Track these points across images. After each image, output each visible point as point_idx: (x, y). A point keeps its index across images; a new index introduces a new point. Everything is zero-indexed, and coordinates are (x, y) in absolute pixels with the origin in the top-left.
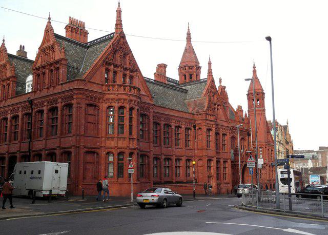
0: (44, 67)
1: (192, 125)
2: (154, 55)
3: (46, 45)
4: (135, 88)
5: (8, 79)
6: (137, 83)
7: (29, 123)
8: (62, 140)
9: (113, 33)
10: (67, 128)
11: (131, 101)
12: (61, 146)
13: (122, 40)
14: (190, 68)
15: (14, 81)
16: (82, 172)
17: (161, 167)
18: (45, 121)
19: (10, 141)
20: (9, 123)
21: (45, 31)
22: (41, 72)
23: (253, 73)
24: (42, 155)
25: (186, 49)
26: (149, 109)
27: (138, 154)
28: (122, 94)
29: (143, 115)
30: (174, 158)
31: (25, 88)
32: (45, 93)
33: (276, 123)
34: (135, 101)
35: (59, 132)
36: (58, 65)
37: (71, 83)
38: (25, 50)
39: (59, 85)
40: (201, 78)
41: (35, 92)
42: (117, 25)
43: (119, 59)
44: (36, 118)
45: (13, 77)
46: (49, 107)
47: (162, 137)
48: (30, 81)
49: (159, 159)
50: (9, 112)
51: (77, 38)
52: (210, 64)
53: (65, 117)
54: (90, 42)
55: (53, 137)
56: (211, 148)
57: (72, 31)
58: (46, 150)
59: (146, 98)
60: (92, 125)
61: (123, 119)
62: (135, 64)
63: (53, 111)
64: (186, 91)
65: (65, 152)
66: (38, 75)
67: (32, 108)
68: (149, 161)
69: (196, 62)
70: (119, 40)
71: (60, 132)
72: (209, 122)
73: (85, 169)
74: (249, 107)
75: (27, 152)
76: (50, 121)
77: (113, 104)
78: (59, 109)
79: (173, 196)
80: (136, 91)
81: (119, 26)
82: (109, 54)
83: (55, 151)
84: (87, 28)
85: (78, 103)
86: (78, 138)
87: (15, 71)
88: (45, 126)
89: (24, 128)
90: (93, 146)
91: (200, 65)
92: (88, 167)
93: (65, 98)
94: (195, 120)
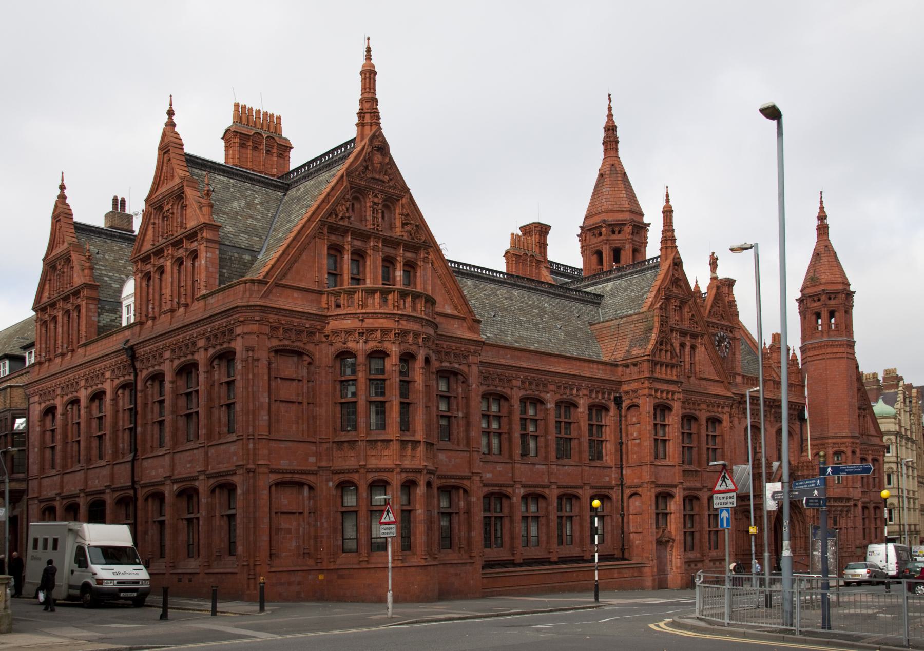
0: (159, 253)
1: (609, 398)
3: (163, 190)
4: (416, 296)
5: (76, 293)
6: (425, 281)
8: (212, 451)
10: (224, 419)
11: (405, 333)
12: (210, 471)
13: (378, 158)
14: (615, 229)
15: (94, 299)
16: (265, 538)
19: (89, 460)
21: (160, 149)
22: (154, 266)
23: (819, 235)
24: (78, 505)
25: (601, 175)
27: (429, 484)
29: (446, 374)
30: (553, 493)
31: (121, 317)
32: (164, 324)
34: (416, 335)
35: (203, 432)
36: (195, 244)
38: (127, 212)
39: (198, 299)
40: (648, 257)
43: (369, 215)
44: (146, 397)
45: (86, 286)
46: (176, 362)
47: (552, 437)
49: (508, 497)
50: (82, 383)
51: (266, 165)
52: (668, 212)
56: (667, 462)
57: (243, 145)
58: (175, 482)
60: (294, 407)
62: (421, 226)
63: (189, 374)
64: (596, 300)
65: (221, 486)
66: (148, 276)
67: (135, 370)
68: (469, 504)
69: (631, 211)
70: (369, 159)
71: (204, 432)
72: (664, 387)
73: (274, 531)
74: (803, 339)
76: (182, 402)
78: (201, 369)
79: (393, 590)
80: (420, 305)
81: (368, 118)
82: (337, 203)
83: (197, 483)
85: (249, 349)
86: (251, 446)
87: (92, 268)
89: (121, 423)
90: (295, 466)
91: (852, 289)
92: (283, 525)
93: (216, 336)
94: (620, 383)
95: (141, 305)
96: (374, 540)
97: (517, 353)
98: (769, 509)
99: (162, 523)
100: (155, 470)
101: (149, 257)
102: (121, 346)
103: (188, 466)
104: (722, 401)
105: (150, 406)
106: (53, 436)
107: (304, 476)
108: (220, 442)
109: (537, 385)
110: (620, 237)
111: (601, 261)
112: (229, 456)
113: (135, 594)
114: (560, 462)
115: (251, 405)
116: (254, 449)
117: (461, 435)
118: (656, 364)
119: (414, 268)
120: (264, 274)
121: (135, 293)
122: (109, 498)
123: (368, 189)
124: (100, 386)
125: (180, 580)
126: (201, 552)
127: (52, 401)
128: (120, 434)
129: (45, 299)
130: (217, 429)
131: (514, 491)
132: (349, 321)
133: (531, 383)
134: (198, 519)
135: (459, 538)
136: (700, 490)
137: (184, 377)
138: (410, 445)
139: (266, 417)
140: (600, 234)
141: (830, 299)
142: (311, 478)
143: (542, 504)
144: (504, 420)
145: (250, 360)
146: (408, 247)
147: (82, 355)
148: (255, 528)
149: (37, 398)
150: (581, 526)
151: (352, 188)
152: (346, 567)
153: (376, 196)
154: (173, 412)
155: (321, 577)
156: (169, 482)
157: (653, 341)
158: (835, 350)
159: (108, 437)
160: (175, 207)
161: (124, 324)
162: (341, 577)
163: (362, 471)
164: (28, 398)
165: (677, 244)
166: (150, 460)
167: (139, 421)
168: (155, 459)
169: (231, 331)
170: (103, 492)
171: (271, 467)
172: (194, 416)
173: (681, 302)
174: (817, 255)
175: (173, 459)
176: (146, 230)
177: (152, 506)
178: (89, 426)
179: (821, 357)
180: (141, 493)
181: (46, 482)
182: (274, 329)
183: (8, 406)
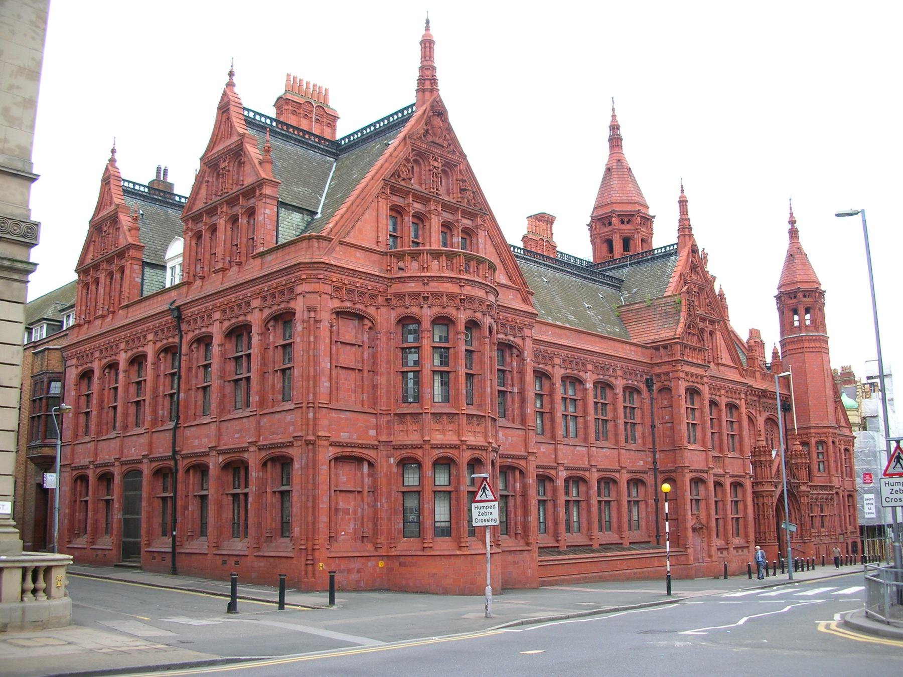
0: (212, 211)
2: (532, 182)
3: (220, 147)
6: (485, 249)
7: (173, 375)
8: (264, 421)
9: (411, 106)
10: (279, 386)
13: (437, 121)
14: (620, 226)
16: (324, 518)
17: (555, 506)
19: (125, 428)
20: (121, 376)
21: (219, 108)
24: (113, 475)
25: (608, 170)
26: (521, 329)
28: (440, 279)
29: (505, 347)
30: (594, 476)
35: (254, 398)
38: (170, 179)
39: (254, 257)
42: (421, 81)
46: (226, 324)
47: (591, 418)
48: (177, 256)
50: (122, 346)
53: (271, 352)
55: (239, 414)
58: (220, 453)
59: (511, 295)
60: (352, 374)
62: (477, 192)
63: (239, 336)
65: (274, 460)
66: (198, 236)
67: (181, 331)
68: (525, 487)
71: (257, 398)
73: (334, 511)
76: (231, 366)
77: (451, 311)
78: (255, 330)
81: (428, 85)
83: (246, 455)
84: (335, 103)
85: (310, 310)
86: (311, 415)
89: (161, 388)
90: (355, 439)
91: (651, 212)
92: (342, 505)
95: (189, 264)
96: (437, 524)
98: (54, 475)
99: (203, 498)
100: (198, 440)
101: (201, 215)
102: (166, 307)
103: (236, 436)
104: (739, 387)
105: (194, 371)
106: (88, 401)
107: (365, 451)
109: (577, 364)
110: (628, 227)
111: (611, 250)
112: (283, 427)
114: (599, 444)
115: (312, 370)
116: (315, 418)
117: (516, 412)
118: (685, 347)
119: (470, 235)
120: (328, 230)
121: (184, 253)
123: (423, 159)
124: (140, 349)
125: (224, 562)
126: (250, 532)
127: (89, 365)
128: (160, 400)
129: (88, 261)
130: (271, 397)
131: (557, 473)
132: (413, 285)
133: (571, 362)
134: (246, 495)
135: (516, 524)
136: (723, 476)
137: (234, 340)
139: (327, 384)
140: (610, 224)
141: (805, 296)
142: (372, 453)
143: (642, 490)
144: (546, 399)
145: (312, 320)
146: (467, 214)
147: (123, 318)
148: (314, 507)
149: (74, 361)
151: (413, 150)
152: (408, 553)
153: (435, 160)
155: (381, 564)
156: (214, 453)
157: (681, 325)
158: (812, 345)
159: (147, 402)
160: (232, 164)
161: (168, 285)
162: (401, 564)
163: (427, 447)
164: (65, 360)
165: (693, 232)
166: (193, 429)
167: (183, 386)
169: (291, 290)
170: (140, 462)
171: (332, 439)
172: (243, 383)
173: (700, 289)
174: (791, 256)
175: (219, 430)
176: (200, 188)
177: (193, 478)
178: (127, 391)
179: (817, 350)
180: (182, 464)
181: (79, 449)
182: (337, 289)
183: (44, 368)
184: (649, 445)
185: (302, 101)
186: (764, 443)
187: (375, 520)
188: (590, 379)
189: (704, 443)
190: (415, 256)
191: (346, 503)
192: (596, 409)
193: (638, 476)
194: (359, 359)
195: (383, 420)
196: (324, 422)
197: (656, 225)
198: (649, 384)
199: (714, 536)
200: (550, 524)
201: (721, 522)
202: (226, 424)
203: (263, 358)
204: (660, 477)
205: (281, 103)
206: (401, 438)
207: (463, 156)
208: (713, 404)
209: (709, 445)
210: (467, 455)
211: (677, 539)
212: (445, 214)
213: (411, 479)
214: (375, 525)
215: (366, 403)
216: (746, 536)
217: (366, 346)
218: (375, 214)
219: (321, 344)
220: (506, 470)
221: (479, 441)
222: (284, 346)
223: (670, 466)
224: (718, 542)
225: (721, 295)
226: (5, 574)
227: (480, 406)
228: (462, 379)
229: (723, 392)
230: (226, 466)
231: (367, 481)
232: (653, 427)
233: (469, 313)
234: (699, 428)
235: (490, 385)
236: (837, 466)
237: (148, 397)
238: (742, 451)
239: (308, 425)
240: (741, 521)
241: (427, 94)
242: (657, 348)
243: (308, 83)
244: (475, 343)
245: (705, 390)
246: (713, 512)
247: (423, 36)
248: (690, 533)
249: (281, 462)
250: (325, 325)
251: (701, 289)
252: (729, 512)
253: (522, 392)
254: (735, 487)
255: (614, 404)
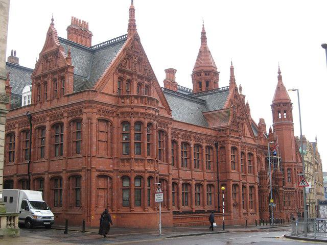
0: (45, 76)
2: (170, 58)
3: (48, 50)
8: (69, 161)
10: (75, 148)
14: (205, 75)
18: (47, 139)
21: (47, 34)
25: (200, 52)
26: (167, 125)
28: (151, 108)
29: (161, 132)
30: (206, 183)
32: (47, 106)
33: (303, 139)
37: (79, 94)
38: (17, 56)
39: (65, 96)
40: (219, 87)
41: (35, 105)
42: (130, 26)
44: (35, 136)
46: (52, 122)
47: (205, 161)
51: (78, 40)
54: (95, 46)
55: (58, 158)
61: (140, 137)
65: (73, 176)
66: (39, 85)
68: (168, 187)
75: (26, 175)
76: (54, 139)
77: (142, 119)
78: (65, 125)
81: (132, 28)
83: (61, 175)
85: (89, 119)
86: (89, 159)
88: (47, 146)
91: (218, 70)
92: (100, 194)
93: (73, 113)
97: (180, 124)
103: (57, 167)
104: (253, 146)
105: (37, 140)
107: (109, 173)
108: (74, 157)
110: (208, 77)
111: (201, 86)
112: (77, 163)
113: (49, 223)
115: (89, 142)
122: (15, 179)
138: (139, 160)
139: (95, 148)
140: (201, 75)
143: (212, 189)
146: (147, 79)
150: (203, 198)
154: (50, 143)
167: (32, 146)
168: (39, 163)
169: (81, 111)
172: (59, 146)
174: (278, 88)
175: (49, 164)
180: (32, 178)
184: (216, 170)
185: (78, 28)
186: (264, 169)
187: (112, 200)
188: (192, 143)
189: (238, 170)
190: (128, 97)
191: (102, 193)
192: (195, 155)
193: (199, 182)
194: (106, 137)
195: (115, 161)
196: (94, 162)
197: (221, 77)
198: (216, 145)
199: (242, 208)
200: (176, 202)
201: (245, 202)
202: (52, 162)
203: (68, 137)
204: (220, 184)
205: (70, 30)
206: (122, 168)
207: (146, 56)
208: (242, 153)
209: (240, 171)
210: (148, 175)
211: (227, 209)
212: (138, 80)
213: (126, 184)
214: (112, 202)
215: (109, 155)
216: (255, 209)
217: (109, 133)
218: (112, 81)
219: (94, 133)
220: (161, 180)
221: (152, 169)
222: (77, 132)
223: (224, 179)
224: (244, 211)
225: (248, 104)
226: (2, 218)
227: (153, 156)
228: (146, 146)
229: (247, 148)
230: (52, 179)
231: (109, 185)
232: (217, 163)
233: (149, 120)
234: (236, 164)
235: (156, 146)
236: (296, 180)
237: (16, 151)
238: (254, 174)
239: (88, 163)
240: (253, 203)
241: (132, 31)
242: (219, 131)
243: (80, 20)
244: (151, 132)
245: (239, 148)
246: (242, 198)
247: (131, 7)
248: (232, 207)
249: (75, 177)
250: (94, 125)
251: (238, 106)
252: (248, 198)
253: (167, 150)
254: (251, 188)
255: (202, 153)
